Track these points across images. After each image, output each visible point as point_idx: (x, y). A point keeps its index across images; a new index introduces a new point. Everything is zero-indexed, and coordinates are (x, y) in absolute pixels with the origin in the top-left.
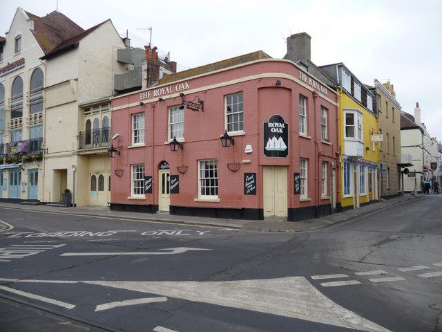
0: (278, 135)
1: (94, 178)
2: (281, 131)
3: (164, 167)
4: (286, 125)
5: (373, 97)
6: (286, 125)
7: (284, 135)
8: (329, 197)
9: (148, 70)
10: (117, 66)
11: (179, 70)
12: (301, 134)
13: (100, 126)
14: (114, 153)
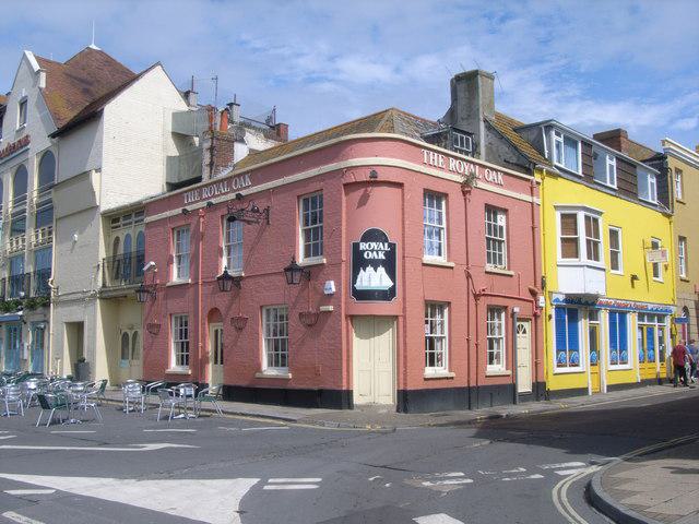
0: (375, 264)
1: (125, 336)
2: (382, 256)
4: (391, 245)
5: (658, 176)
6: (391, 245)
7: (389, 264)
8: (509, 372)
10: (171, 142)
11: (293, 135)
12: (428, 258)
13: (133, 249)
14: (230, 283)
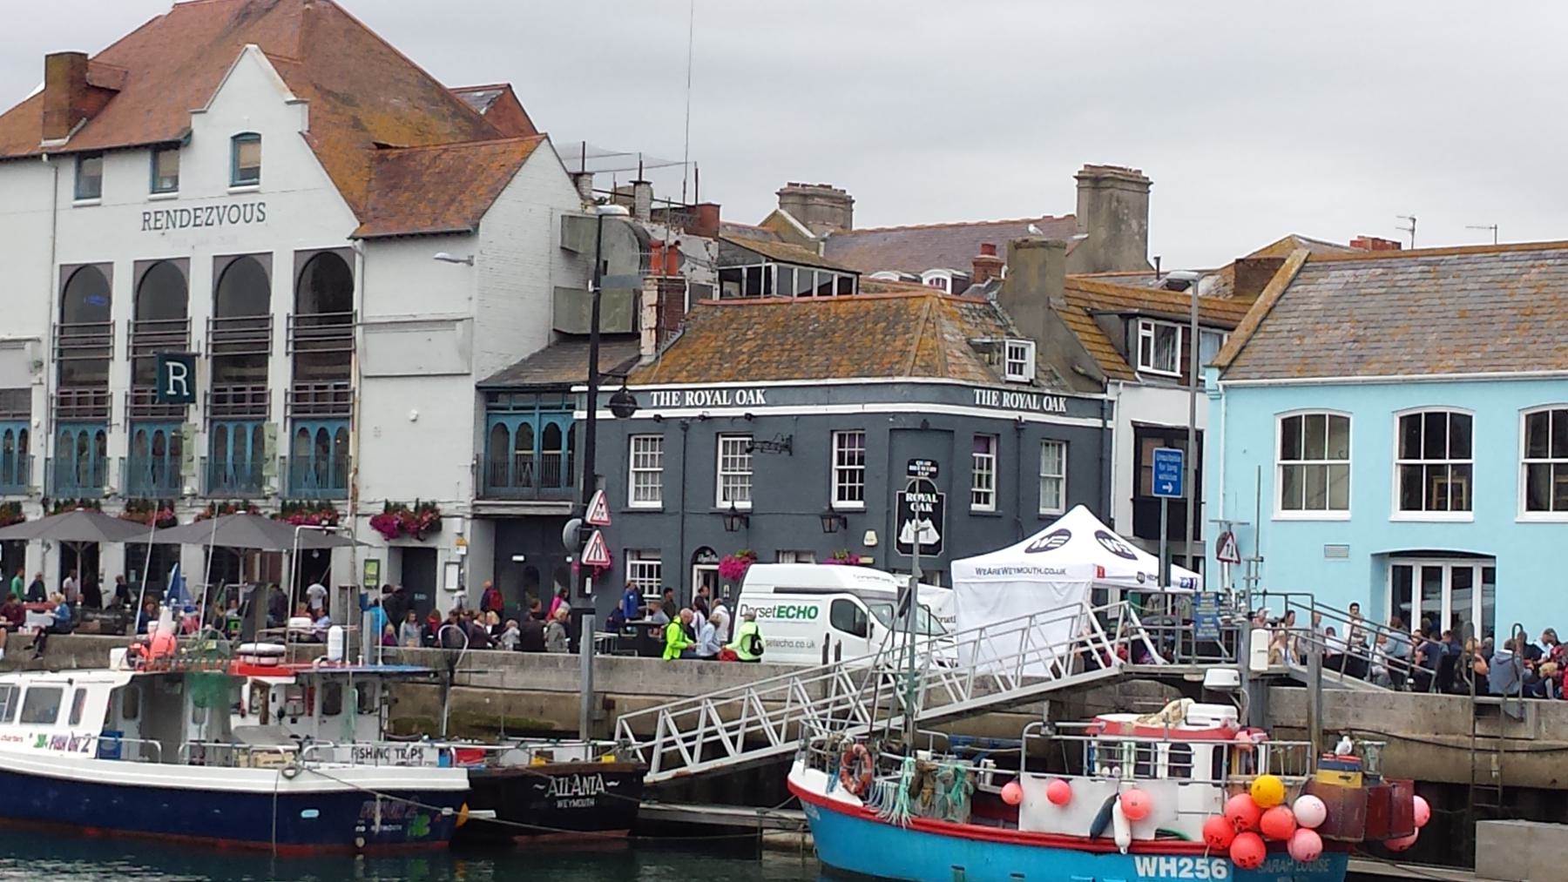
0: (923, 516)
2: (929, 508)
3: (706, 560)
6: (939, 498)
9: (659, 307)
